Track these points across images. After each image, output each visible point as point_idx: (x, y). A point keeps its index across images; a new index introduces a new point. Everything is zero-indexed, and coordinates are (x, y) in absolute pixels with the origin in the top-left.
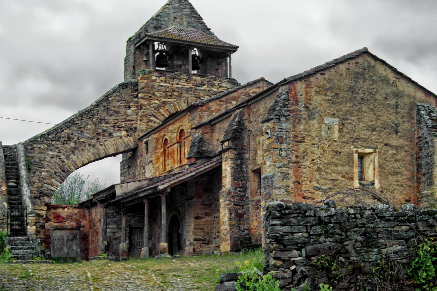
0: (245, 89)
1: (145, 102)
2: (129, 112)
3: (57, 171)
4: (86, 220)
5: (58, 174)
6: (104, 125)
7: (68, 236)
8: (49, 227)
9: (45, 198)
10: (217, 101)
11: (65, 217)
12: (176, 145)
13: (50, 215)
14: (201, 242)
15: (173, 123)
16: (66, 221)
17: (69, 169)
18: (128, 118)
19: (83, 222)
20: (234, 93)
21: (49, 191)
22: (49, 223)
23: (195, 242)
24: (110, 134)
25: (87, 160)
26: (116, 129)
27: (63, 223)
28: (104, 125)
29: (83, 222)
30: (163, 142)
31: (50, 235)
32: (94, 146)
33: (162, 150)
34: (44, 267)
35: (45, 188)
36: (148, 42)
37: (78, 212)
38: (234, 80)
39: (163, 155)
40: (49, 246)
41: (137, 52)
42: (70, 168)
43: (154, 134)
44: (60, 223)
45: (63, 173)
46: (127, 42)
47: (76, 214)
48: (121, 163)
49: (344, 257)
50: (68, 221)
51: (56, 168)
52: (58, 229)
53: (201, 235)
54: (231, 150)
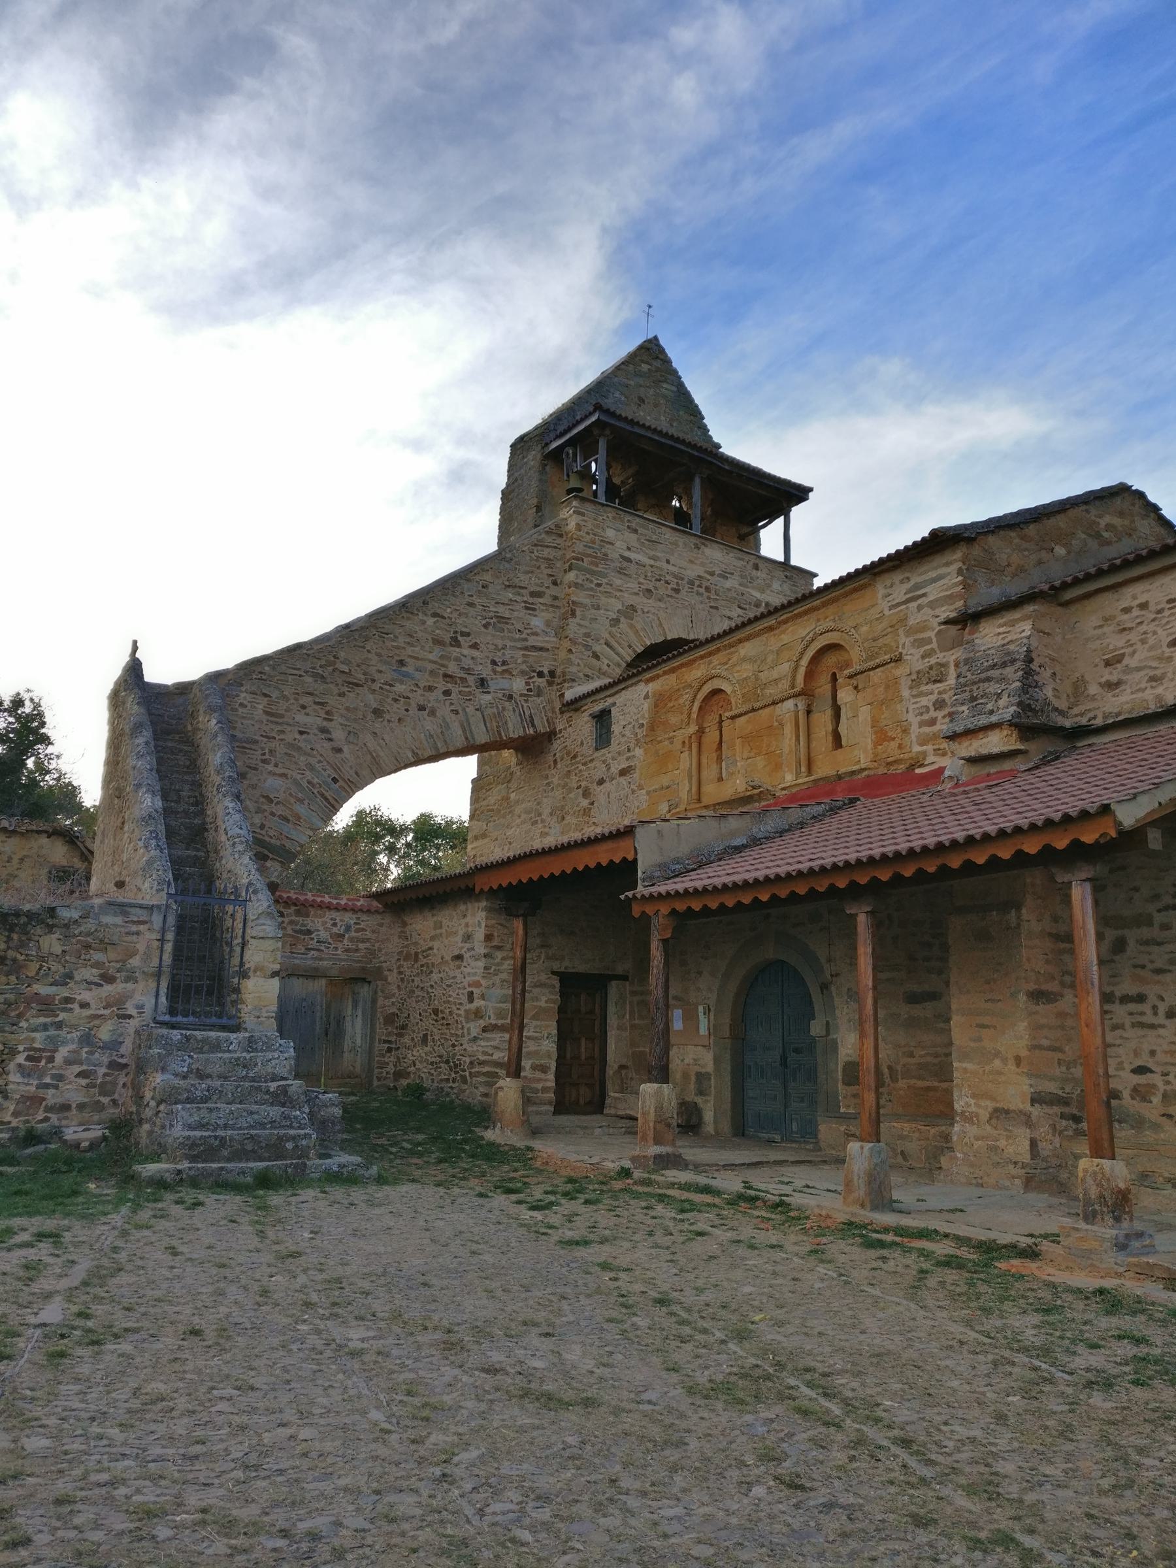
0: (1087, 511)
1: (581, 597)
2: (537, 622)
6: (466, 651)
10: (1013, 534)
12: (789, 704)
14: (1057, 1110)
15: (771, 629)
18: (532, 641)
20: (1059, 517)
23: (1036, 1111)
24: (482, 683)
25: (410, 755)
26: (499, 669)
28: (466, 651)
30: (697, 705)
32: (433, 713)
33: (693, 728)
34: (1015, 1262)
36: (596, 432)
38: (92, 853)
39: (694, 747)
41: (548, 468)
43: (648, 681)
52: (299, 976)
53: (1051, 1079)
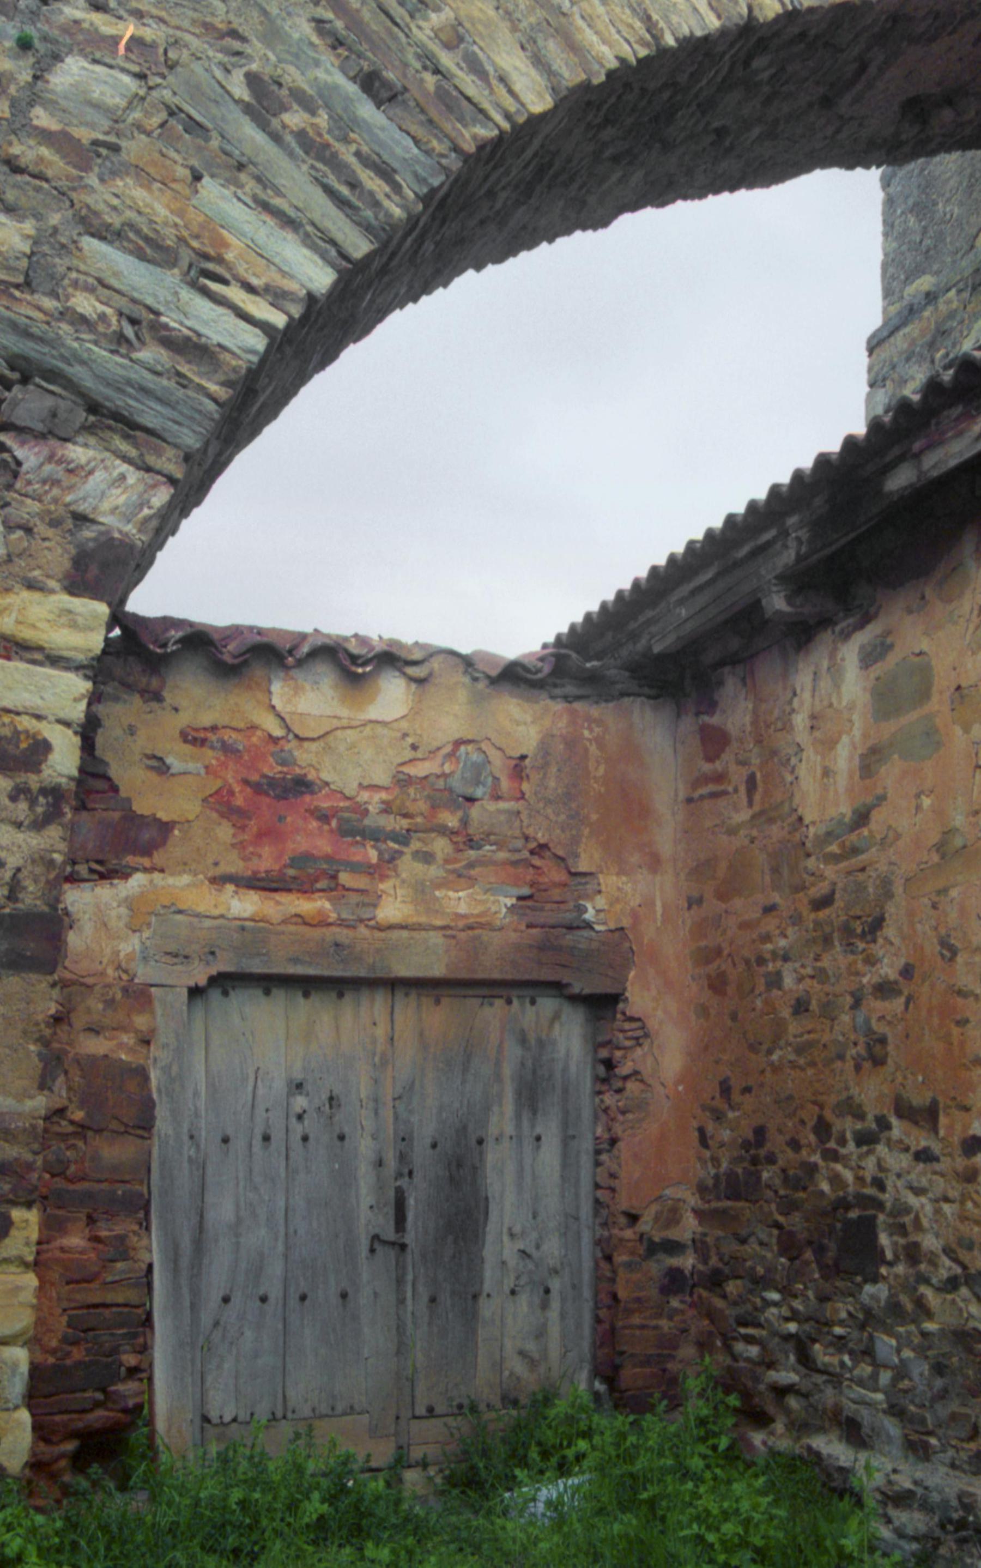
3: (293, 76)
4: (654, 863)
5: (295, 119)
7: (405, 1094)
8: (130, 945)
9: (78, 453)
11: (374, 801)
13: (159, 766)
16: (377, 871)
17: (469, 84)
19: (610, 881)
21: (150, 354)
22: (138, 881)
27: (335, 889)
29: (610, 881)
31: (142, 1074)
35: (85, 304)
37: (544, 747)
40: (122, 1250)
42: (475, 67)
44: (305, 888)
45: (367, 110)
46: (316, 630)
47: (518, 767)
48: (874, 345)
49: (54, 1081)
50: (408, 866)
51: (272, 35)
54: (573, 870)
